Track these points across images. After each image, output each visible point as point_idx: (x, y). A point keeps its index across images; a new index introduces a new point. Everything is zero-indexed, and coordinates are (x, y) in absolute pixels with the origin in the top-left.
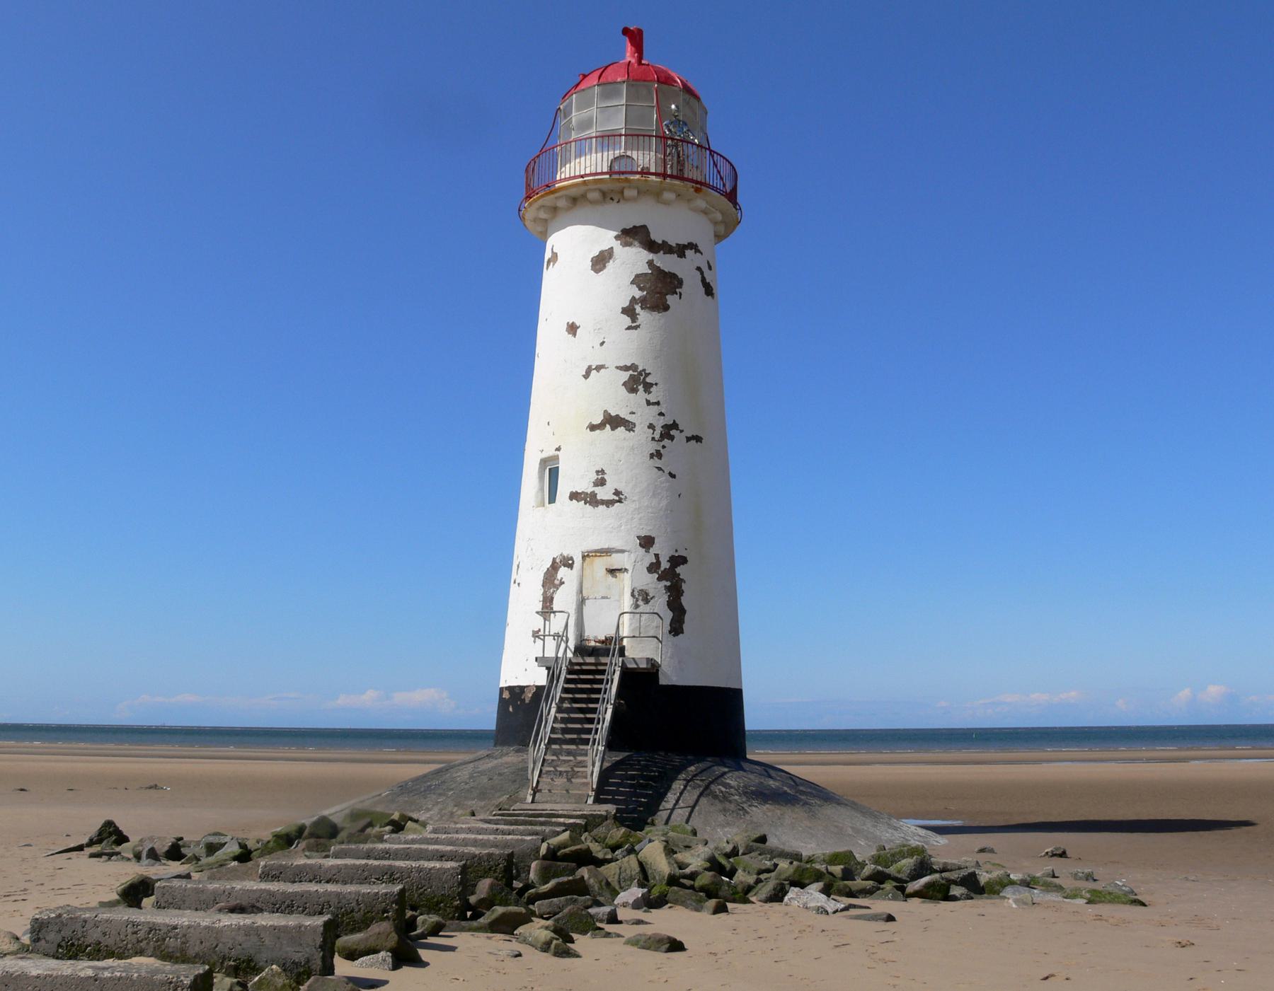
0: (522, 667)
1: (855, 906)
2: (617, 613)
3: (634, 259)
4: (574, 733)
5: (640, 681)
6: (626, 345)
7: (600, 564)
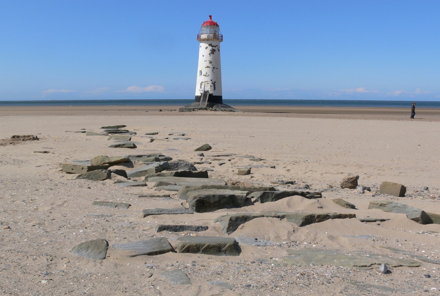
0: (198, 93)
1: (245, 219)
2: (208, 88)
3: (210, 48)
4: (204, 100)
5: (211, 95)
6: (209, 58)
7: (206, 83)
